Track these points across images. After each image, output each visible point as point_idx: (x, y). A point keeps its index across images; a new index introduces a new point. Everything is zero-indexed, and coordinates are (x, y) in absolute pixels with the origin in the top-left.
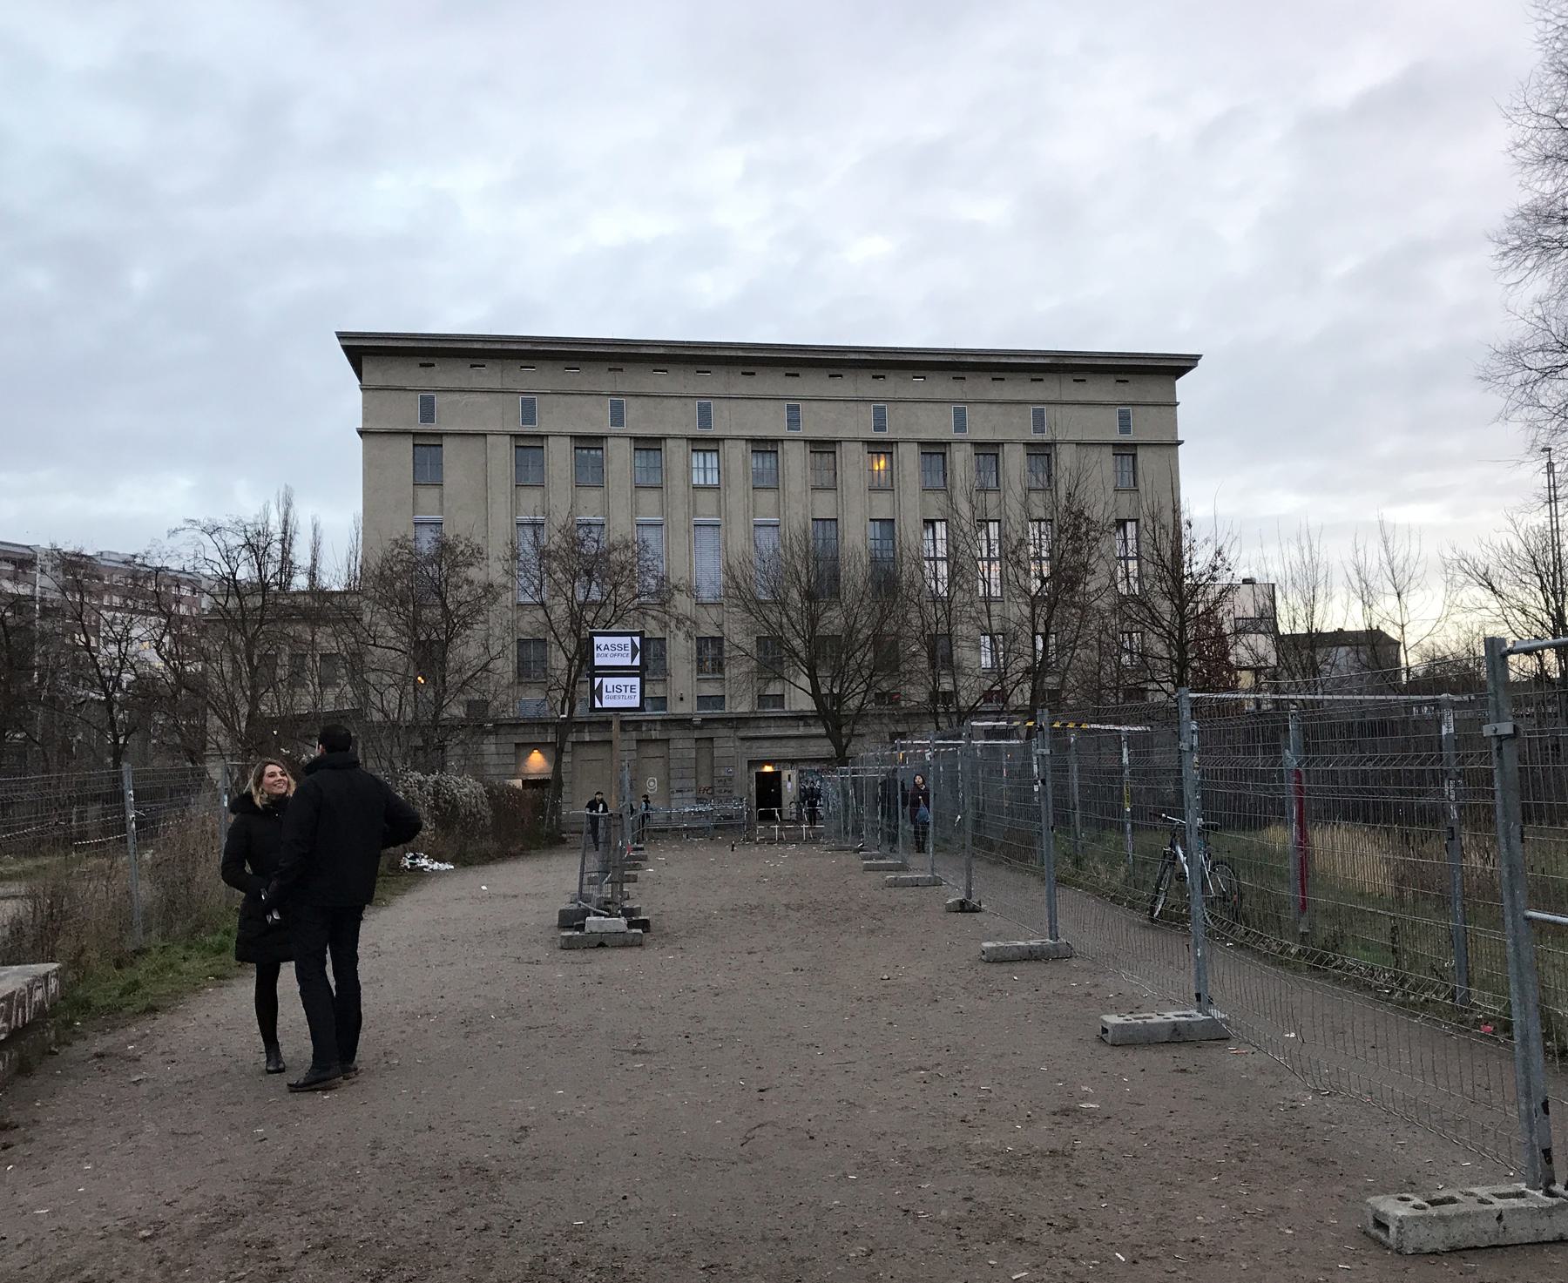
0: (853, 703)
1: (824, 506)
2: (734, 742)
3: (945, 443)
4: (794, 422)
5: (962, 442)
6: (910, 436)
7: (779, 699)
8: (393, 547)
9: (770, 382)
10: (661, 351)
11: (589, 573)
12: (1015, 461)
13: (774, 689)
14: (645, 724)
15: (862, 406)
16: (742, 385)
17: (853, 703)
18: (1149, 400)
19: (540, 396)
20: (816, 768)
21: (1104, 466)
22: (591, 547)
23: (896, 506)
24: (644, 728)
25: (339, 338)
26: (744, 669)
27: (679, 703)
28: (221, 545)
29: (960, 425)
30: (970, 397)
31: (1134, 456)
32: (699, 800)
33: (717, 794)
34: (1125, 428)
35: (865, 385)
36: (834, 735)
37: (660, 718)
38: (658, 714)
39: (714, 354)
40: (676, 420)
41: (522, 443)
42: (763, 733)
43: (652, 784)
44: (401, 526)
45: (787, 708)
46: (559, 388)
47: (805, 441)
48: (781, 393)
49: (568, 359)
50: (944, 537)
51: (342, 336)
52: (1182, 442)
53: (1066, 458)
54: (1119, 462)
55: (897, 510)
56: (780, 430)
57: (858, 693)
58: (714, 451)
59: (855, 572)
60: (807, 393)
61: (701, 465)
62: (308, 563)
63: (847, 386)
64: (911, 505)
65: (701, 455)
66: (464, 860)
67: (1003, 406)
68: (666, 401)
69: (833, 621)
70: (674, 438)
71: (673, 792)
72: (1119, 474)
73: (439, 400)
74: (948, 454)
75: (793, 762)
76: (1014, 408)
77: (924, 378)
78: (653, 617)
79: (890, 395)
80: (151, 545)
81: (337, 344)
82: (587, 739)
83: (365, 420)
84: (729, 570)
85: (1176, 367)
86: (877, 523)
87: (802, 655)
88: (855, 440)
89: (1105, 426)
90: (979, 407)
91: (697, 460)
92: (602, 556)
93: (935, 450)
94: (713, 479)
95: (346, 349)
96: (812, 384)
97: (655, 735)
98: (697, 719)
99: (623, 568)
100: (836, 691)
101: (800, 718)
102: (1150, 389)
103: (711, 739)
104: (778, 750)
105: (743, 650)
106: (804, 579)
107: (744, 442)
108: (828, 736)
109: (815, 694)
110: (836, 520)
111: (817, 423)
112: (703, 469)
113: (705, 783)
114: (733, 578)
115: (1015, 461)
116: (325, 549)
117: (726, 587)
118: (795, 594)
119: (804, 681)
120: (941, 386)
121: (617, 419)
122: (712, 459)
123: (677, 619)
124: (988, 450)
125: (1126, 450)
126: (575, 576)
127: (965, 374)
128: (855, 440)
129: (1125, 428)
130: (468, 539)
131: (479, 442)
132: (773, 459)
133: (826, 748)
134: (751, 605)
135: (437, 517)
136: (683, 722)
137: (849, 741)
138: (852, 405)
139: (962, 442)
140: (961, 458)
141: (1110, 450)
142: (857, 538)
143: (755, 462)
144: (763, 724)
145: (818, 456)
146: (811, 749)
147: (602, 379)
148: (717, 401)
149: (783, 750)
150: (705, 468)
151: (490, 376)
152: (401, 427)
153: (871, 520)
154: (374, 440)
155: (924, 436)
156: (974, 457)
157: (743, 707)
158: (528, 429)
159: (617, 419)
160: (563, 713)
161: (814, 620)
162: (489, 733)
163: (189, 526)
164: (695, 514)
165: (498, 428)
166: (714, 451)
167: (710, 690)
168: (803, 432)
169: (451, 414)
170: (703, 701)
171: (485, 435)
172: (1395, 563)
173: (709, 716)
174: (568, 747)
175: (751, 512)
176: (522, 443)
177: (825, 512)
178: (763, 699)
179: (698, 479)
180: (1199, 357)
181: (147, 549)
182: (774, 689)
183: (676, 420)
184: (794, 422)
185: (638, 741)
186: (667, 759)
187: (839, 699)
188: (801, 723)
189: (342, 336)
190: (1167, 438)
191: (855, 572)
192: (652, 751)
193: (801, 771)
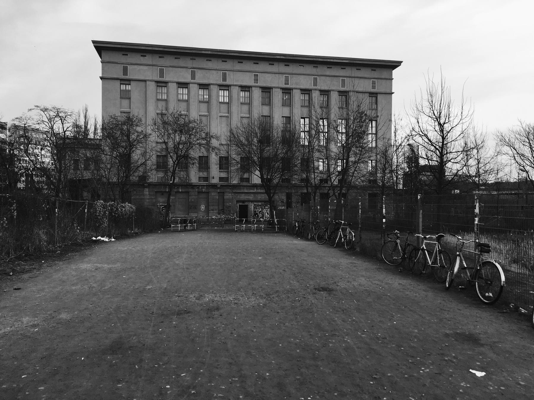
0: (275, 181)
1: (266, 111)
2: (232, 194)
3: (310, 90)
4: (256, 80)
5: (316, 90)
6: (298, 87)
7: (248, 180)
8: (110, 118)
9: (248, 66)
10: (210, 53)
11: (181, 131)
12: (335, 97)
13: (246, 176)
14: (200, 186)
15: (280, 75)
16: (238, 66)
17: (275, 181)
18: (383, 77)
19: (166, 68)
20: (260, 204)
21: (367, 100)
22: (182, 121)
23: (292, 112)
24: (200, 188)
25: (93, 43)
26: (236, 167)
27: (213, 180)
28: (48, 115)
29: (315, 84)
30: (320, 73)
31: (377, 97)
32: (219, 214)
33: (225, 212)
34: (374, 87)
35: (282, 68)
36: (268, 193)
37: (206, 184)
38: (205, 183)
39: (228, 54)
40: (214, 78)
41: (159, 85)
42: (242, 191)
43: (203, 207)
44: (116, 111)
45: (250, 183)
46: (172, 65)
47: (260, 87)
48: (252, 69)
49: (372, 67)
50: (228, 95)
51: (94, 42)
52: (393, 93)
53: (353, 98)
54: (371, 99)
55: (271, 113)
56: (250, 82)
57: (277, 178)
58: (268, 92)
59: (277, 133)
60: (260, 70)
61: (223, 95)
62: (394, 121)
63: (276, 68)
64: (298, 111)
65: (223, 91)
66: (122, 236)
67: (331, 77)
68: (212, 71)
69: (269, 151)
70: (333, 90)
71: (210, 211)
72: (371, 104)
73: (129, 67)
74: (310, 94)
75: (252, 201)
76: (335, 78)
77: (303, 66)
78: (204, 147)
79: (291, 72)
80: (22, 115)
81: (92, 45)
82: (180, 191)
83: (103, 74)
84: (231, 131)
85: (394, 65)
86: (284, 118)
87: (257, 163)
88: (151, 81)
89: (365, 85)
90: (322, 77)
91: (221, 93)
92: (186, 125)
93: (306, 91)
94: (226, 100)
95: (96, 47)
96: (263, 66)
97: (204, 190)
98: (219, 186)
99: (193, 129)
100: (269, 177)
101: (255, 186)
102: (384, 73)
103: (224, 192)
104: (247, 197)
105: (236, 161)
106: (259, 135)
107: (238, 87)
108: (266, 193)
109: (262, 177)
110: (270, 116)
111: (201, 77)
112: (223, 96)
113: (221, 208)
114: (233, 134)
115: (335, 97)
116: (97, 120)
117: (230, 137)
118: (255, 140)
119: (257, 173)
120: (309, 69)
121: (193, 77)
122: (226, 93)
123: (212, 148)
124: (325, 93)
125: (374, 95)
126: (176, 131)
127: (318, 66)
128: (236, 85)
129: (374, 87)
130: (137, 116)
131: (143, 84)
132: (289, 95)
133: (265, 197)
134: (239, 144)
135: (128, 110)
136: (214, 186)
137: (273, 196)
138: (277, 75)
139: (316, 90)
140: (316, 95)
141: (368, 95)
142: (278, 121)
143: (302, 97)
144: (242, 187)
145: (264, 93)
146: (259, 197)
147: (188, 62)
148: (260, 74)
149: (249, 197)
150: (224, 96)
151: (148, 59)
152: (115, 76)
153: (282, 117)
154: (107, 81)
155: (302, 87)
156: (339, 96)
157: (235, 182)
158: (224, 83)
159: (193, 77)
160: (171, 181)
161: (262, 151)
162: (146, 187)
163: (36, 108)
164: (199, 112)
165: (150, 78)
166: (268, 92)
167: (224, 175)
168: (318, 87)
169: (134, 72)
170: (221, 179)
171: (145, 81)
172: (477, 136)
173: (223, 184)
174: (173, 193)
175: (240, 112)
176: (159, 85)
177: (266, 113)
178: (242, 179)
179: (221, 99)
180: (402, 62)
181: (21, 116)
182: (246, 176)
183: (214, 78)
184: (256, 80)
185: (198, 192)
186: (208, 198)
187: (270, 180)
188: (255, 188)
189: (94, 42)
190: (388, 91)
191: (277, 133)
192: (203, 196)
193: (255, 205)
